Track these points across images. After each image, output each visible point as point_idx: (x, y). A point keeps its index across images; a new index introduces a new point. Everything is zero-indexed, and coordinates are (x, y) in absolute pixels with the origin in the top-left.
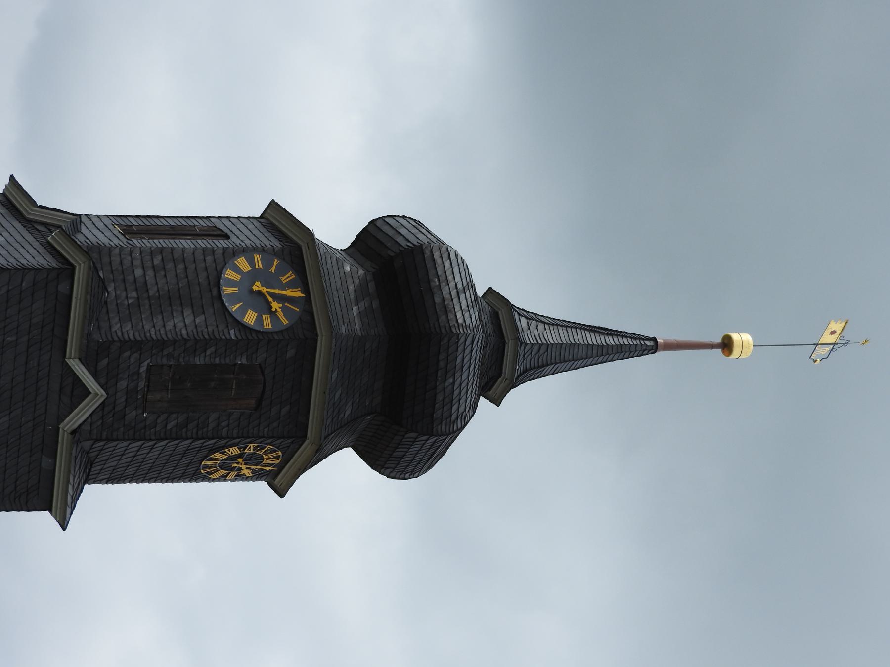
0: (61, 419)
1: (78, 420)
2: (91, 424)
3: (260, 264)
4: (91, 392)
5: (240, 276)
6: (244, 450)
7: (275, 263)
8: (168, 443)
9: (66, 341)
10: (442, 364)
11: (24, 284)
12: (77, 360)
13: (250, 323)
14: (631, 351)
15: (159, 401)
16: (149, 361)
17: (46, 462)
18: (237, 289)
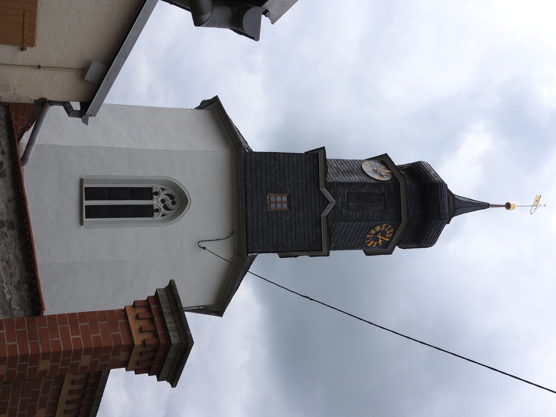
0: (321, 213)
1: (328, 211)
2: (331, 215)
4: (330, 201)
6: (377, 243)
8: (357, 223)
9: (319, 182)
10: (440, 193)
11: (302, 159)
12: (324, 188)
15: (352, 206)
16: (347, 191)
17: (318, 230)
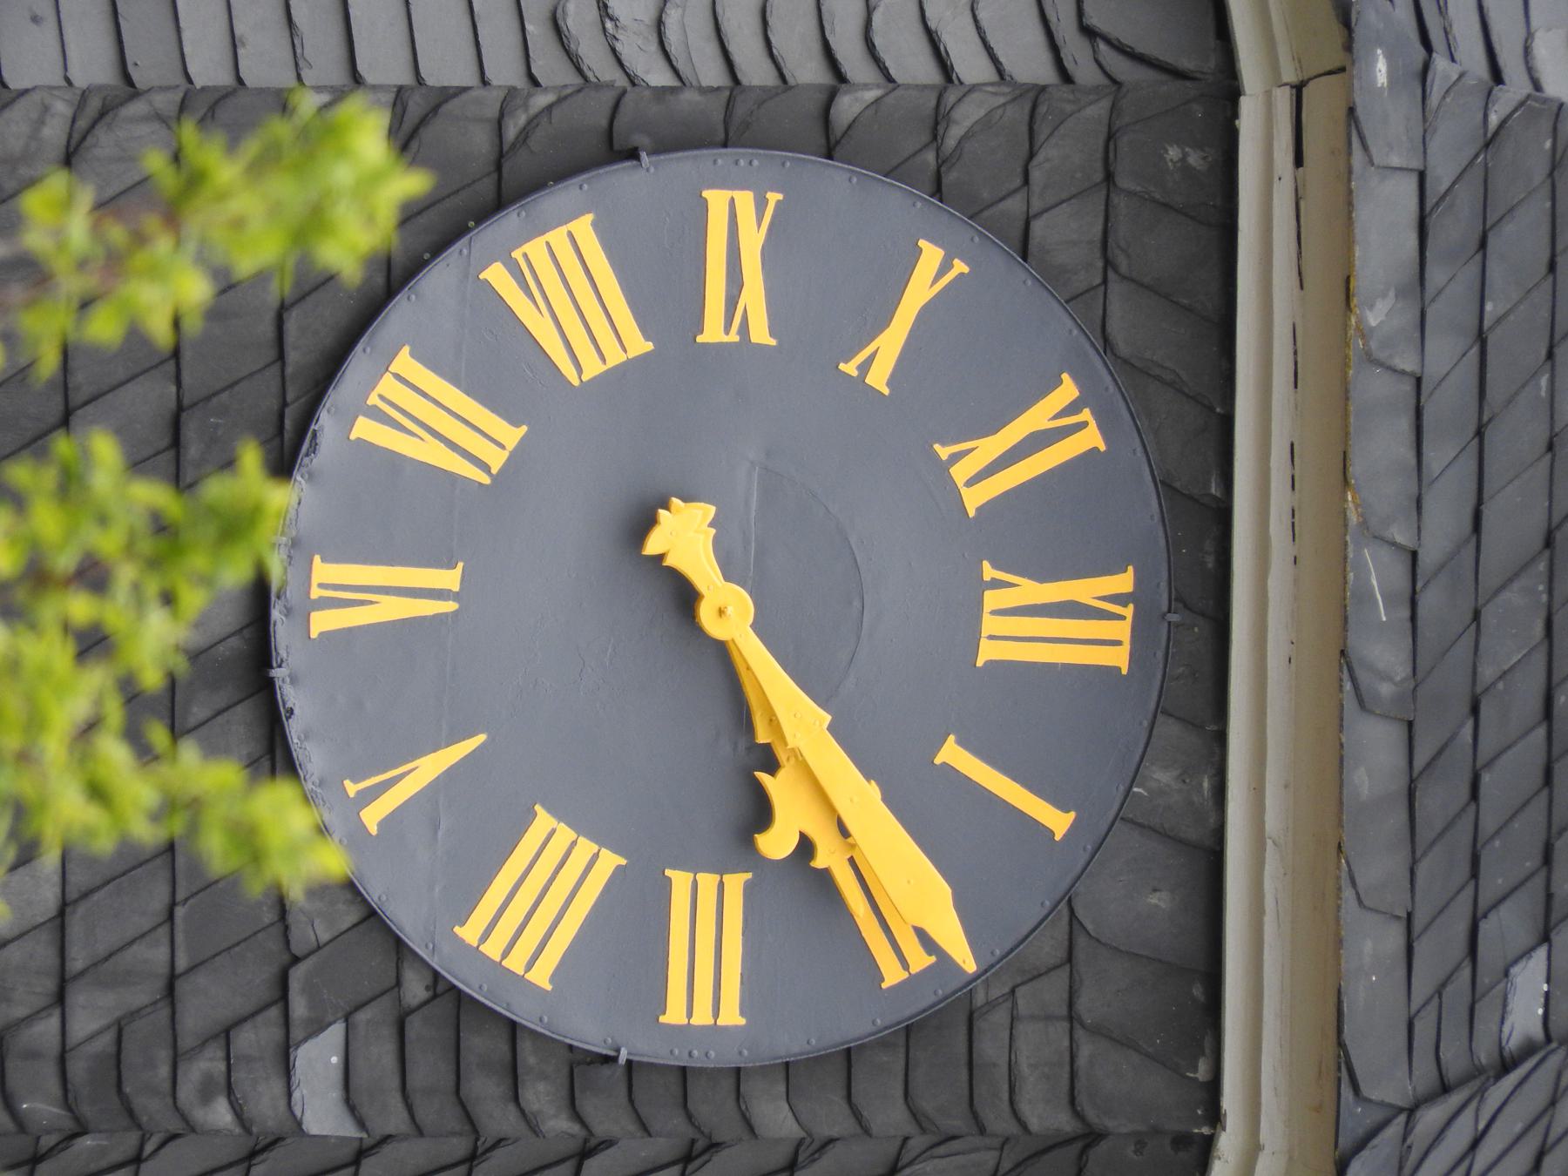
3: (754, 297)
5: (512, 435)
7: (920, 290)
13: (515, 963)
14: (297, 949)
18: (450, 579)
